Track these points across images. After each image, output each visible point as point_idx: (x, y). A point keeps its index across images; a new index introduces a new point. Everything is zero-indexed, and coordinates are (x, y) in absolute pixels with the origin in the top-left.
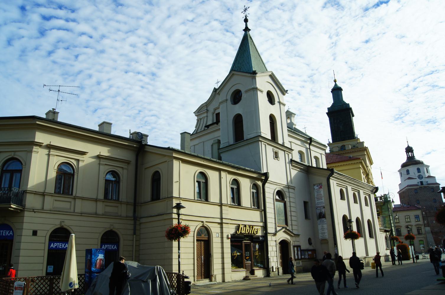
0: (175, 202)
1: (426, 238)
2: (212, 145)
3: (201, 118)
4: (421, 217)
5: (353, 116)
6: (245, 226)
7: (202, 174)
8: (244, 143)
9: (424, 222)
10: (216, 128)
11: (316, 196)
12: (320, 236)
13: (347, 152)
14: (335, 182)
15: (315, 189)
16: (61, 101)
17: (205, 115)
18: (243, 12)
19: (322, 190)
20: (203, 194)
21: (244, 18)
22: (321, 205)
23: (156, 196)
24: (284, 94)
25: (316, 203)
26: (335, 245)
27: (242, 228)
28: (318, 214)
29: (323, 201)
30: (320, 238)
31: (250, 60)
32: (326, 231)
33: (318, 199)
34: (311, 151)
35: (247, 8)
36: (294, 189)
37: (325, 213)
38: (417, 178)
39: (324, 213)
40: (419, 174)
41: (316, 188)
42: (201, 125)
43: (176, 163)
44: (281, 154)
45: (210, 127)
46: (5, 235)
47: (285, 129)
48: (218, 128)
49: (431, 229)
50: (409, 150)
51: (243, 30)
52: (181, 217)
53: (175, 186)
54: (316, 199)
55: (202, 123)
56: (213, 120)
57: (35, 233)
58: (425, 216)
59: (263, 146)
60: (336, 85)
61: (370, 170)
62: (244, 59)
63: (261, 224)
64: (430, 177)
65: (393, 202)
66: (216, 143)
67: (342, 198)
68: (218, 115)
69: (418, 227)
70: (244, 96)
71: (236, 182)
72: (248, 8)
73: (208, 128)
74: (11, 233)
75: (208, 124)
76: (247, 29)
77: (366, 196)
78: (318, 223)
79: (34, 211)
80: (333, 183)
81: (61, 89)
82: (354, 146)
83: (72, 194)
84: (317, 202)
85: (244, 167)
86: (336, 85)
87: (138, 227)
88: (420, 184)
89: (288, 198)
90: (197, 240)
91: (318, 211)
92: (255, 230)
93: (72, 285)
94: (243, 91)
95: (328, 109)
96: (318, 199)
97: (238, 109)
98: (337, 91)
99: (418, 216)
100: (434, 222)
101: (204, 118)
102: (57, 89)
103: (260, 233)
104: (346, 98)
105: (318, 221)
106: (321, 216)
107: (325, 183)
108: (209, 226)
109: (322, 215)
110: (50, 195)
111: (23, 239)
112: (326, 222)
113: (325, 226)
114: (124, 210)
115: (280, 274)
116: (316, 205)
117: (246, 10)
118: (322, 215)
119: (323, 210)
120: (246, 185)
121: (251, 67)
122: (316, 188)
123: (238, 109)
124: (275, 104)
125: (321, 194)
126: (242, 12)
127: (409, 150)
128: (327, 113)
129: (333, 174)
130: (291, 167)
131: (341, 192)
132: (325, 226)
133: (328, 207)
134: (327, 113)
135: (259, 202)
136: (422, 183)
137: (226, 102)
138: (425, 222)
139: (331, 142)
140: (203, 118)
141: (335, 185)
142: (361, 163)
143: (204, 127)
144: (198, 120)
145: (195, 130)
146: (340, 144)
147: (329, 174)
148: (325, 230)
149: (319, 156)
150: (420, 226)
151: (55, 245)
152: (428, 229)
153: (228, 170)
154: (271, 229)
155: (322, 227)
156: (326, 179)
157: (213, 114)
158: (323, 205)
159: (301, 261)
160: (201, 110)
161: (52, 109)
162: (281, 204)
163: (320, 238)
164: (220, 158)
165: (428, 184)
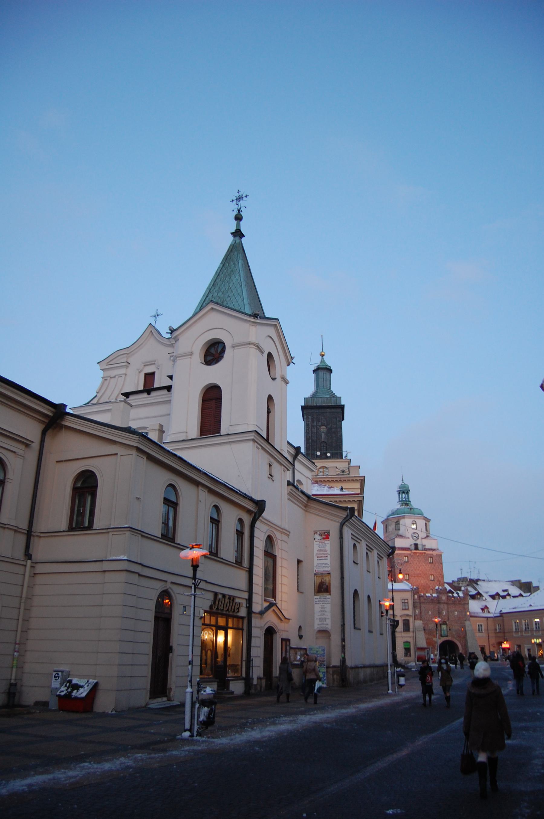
1: (415, 638)
5: (343, 419)
6: (224, 596)
7: (216, 507)
8: (220, 440)
10: (143, 401)
11: (316, 552)
13: (330, 480)
14: (350, 532)
15: (316, 540)
17: (123, 371)
18: (235, 202)
19: (327, 542)
21: (236, 212)
29: (328, 561)
32: (328, 615)
34: (296, 471)
35: (244, 195)
36: (288, 536)
37: (330, 584)
44: (277, 469)
49: (423, 624)
50: (404, 491)
51: (232, 233)
58: (418, 601)
60: (323, 361)
62: (231, 285)
63: (246, 595)
69: (404, 618)
72: (246, 196)
76: (238, 234)
78: (315, 600)
84: (316, 562)
86: (323, 361)
95: (306, 399)
98: (323, 371)
100: (430, 612)
101: (120, 376)
104: (339, 386)
105: (316, 597)
109: (324, 586)
112: (328, 600)
113: (328, 607)
116: (315, 569)
118: (324, 586)
119: (327, 579)
125: (326, 550)
127: (404, 491)
128: (302, 407)
129: (351, 518)
136: (416, 545)
138: (417, 611)
147: (345, 516)
148: (325, 614)
150: (408, 618)
153: (210, 488)
154: (257, 607)
155: (322, 608)
156: (338, 525)
159: (437, 665)
160: (115, 360)
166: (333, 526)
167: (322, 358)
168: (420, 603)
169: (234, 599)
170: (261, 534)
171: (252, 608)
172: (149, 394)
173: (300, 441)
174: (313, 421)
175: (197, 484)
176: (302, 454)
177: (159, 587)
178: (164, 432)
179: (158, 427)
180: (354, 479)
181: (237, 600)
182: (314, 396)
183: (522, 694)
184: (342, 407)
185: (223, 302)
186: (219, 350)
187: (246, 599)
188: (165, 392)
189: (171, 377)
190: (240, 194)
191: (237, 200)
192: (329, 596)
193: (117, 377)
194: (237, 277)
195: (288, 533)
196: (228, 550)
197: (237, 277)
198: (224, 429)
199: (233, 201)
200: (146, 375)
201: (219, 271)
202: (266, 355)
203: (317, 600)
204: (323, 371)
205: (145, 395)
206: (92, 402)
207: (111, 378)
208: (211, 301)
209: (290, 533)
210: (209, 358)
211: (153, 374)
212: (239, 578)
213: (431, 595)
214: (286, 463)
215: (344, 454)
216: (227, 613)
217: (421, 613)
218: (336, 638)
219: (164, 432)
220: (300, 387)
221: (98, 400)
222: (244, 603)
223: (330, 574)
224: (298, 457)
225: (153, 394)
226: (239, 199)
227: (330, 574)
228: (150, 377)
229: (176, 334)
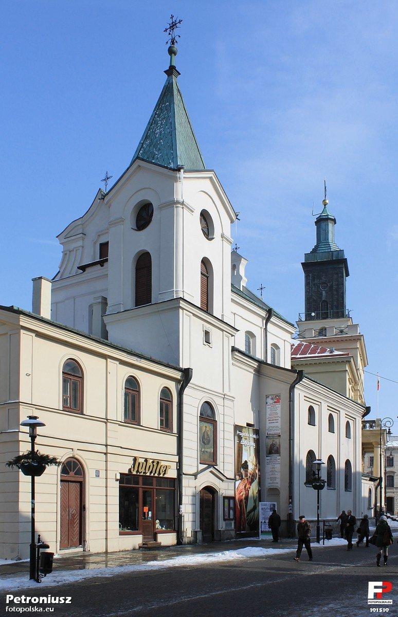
0: (24, 414)
2: (91, 306)
3: (71, 248)
5: (347, 275)
11: (268, 416)
14: (302, 394)
15: (268, 404)
17: (80, 243)
18: (168, 31)
19: (279, 406)
20: (74, 401)
21: (169, 45)
22: (275, 432)
25: (267, 427)
26: (290, 499)
27: (139, 464)
29: (279, 424)
31: (173, 139)
32: (278, 475)
34: (268, 333)
35: (178, 21)
41: (270, 401)
43: (26, 339)
45: (88, 270)
47: (228, 287)
48: (104, 274)
51: (165, 72)
52: (37, 440)
53: (24, 381)
54: (267, 420)
59: (186, 319)
61: (360, 375)
63: (176, 459)
65: (389, 433)
67: (311, 422)
68: (104, 247)
71: (132, 385)
73: (84, 271)
77: (350, 421)
80: (299, 392)
89: (221, 416)
90: (62, 481)
91: (270, 442)
92: (162, 468)
97: (144, 241)
108: (83, 456)
109: (275, 448)
115: (198, 541)
117: (173, 25)
118: (275, 448)
119: (277, 441)
120: (151, 389)
122: (270, 401)
123: (144, 241)
124: (213, 238)
125: (277, 414)
126: (166, 30)
129: (301, 380)
130: (231, 361)
131: (311, 410)
132: (278, 467)
133: (286, 437)
135: (169, 418)
139: (303, 319)
140: (75, 250)
141: (302, 398)
142: (349, 362)
146: (319, 324)
149: (280, 344)
154: (185, 470)
157: (95, 243)
158: (277, 432)
164: (105, 334)
171: (182, 470)
174: (314, 279)
175: (105, 357)
179: (100, 300)
180: (352, 338)
181: (162, 463)
182: (315, 250)
183: (368, 546)
184: (344, 261)
187: (177, 462)
190: (174, 19)
191: (170, 28)
192: (279, 457)
193: (75, 250)
195: (232, 399)
199: (166, 30)
201: (151, 121)
203: (268, 461)
206: (56, 279)
207: (70, 252)
210: (143, 222)
211: (107, 243)
214: (229, 328)
216: (152, 475)
218: (284, 494)
222: (174, 466)
223: (280, 436)
224: (271, 319)
226: (173, 26)
227: (280, 436)
229: (106, 199)
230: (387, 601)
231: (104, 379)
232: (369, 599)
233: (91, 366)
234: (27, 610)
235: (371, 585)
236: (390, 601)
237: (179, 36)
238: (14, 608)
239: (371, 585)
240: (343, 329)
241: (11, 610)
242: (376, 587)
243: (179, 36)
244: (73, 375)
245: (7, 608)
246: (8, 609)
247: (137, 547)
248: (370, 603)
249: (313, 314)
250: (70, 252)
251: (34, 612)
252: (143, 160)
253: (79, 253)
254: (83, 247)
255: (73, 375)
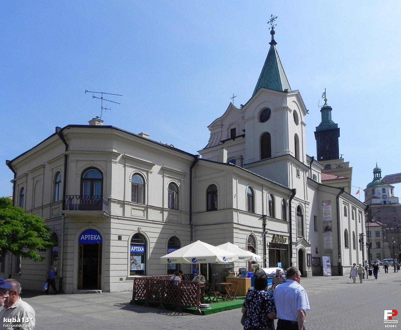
1: (383, 252)
4: (381, 234)
6: (278, 235)
9: (383, 238)
11: (324, 211)
12: (325, 247)
13: (332, 171)
14: (342, 200)
15: (324, 205)
16: (106, 109)
18: (270, 23)
21: (271, 30)
23: (212, 206)
24: (305, 114)
28: (325, 228)
29: (331, 216)
30: (325, 248)
32: (331, 242)
33: (326, 214)
37: (331, 227)
38: (381, 198)
39: (330, 227)
40: (384, 194)
42: (215, 140)
45: (226, 142)
46: (93, 239)
51: (269, 43)
53: (234, 200)
54: (324, 214)
55: (216, 137)
56: (228, 135)
57: (120, 238)
59: (290, 166)
60: (326, 104)
63: (288, 235)
64: (393, 197)
66: (239, 158)
70: (273, 114)
74: (99, 237)
75: (223, 139)
76: (273, 43)
79: (118, 218)
81: (104, 96)
82: (339, 166)
83: (144, 203)
84: (324, 216)
85: (279, 184)
87: (194, 234)
88: (383, 203)
91: (325, 225)
93: (13, 307)
94: (272, 109)
96: (325, 214)
97: (265, 127)
98: (326, 110)
99: (378, 232)
102: (100, 96)
103: (287, 243)
104: (335, 118)
105: (324, 233)
106: (327, 229)
107: (334, 200)
110: (129, 203)
111: (112, 243)
113: (331, 238)
114: (185, 219)
119: (330, 224)
120: (279, 201)
121: (280, 85)
122: (324, 204)
123: (265, 127)
126: (269, 22)
134: (231, 106)
136: (385, 202)
137: (253, 120)
138: (385, 237)
143: (218, 141)
144: (212, 135)
145: (208, 144)
149: (316, 174)
150: (379, 241)
151: (134, 249)
152: (386, 244)
154: (294, 240)
161: (96, 117)
162: (300, 218)
163: (325, 248)
165: (391, 204)
166: (333, 198)
167: (326, 102)
168: (387, 233)
169: (283, 237)
170: (294, 204)
172: (234, 140)
173: (314, 154)
176: (316, 161)
177: (249, 233)
178: (243, 159)
179: (240, 157)
182: (321, 125)
185: (267, 86)
186: (268, 113)
188: (242, 138)
189: (244, 131)
194: (274, 69)
196: (279, 214)
197: (274, 69)
198: (273, 154)
200: (232, 130)
202: (292, 112)
204: (326, 110)
205: (232, 140)
208: (261, 87)
209: (309, 203)
211: (235, 129)
212: (283, 228)
213: (394, 228)
215: (340, 156)
217: (387, 238)
219: (243, 159)
220: (314, 120)
221: (210, 146)
225: (236, 139)
226: (272, 20)
228: (233, 131)
230: (395, 321)
231: (262, 199)
232: (385, 320)
233: (258, 194)
234: (15, 326)
235: (386, 312)
236: (397, 321)
237: (276, 25)
238: (8, 325)
239: (386, 312)
240: (340, 165)
241: (6, 326)
242: (388, 313)
243: (276, 25)
244: (251, 198)
245: (4, 325)
246: (5, 326)
247: (127, 290)
248: (385, 322)
249: (322, 158)
250: (214, 134)
251: (20, 327)
252: (264, 88)
253: (220, 135)
254: (222, 131)
255: (251, 198)
